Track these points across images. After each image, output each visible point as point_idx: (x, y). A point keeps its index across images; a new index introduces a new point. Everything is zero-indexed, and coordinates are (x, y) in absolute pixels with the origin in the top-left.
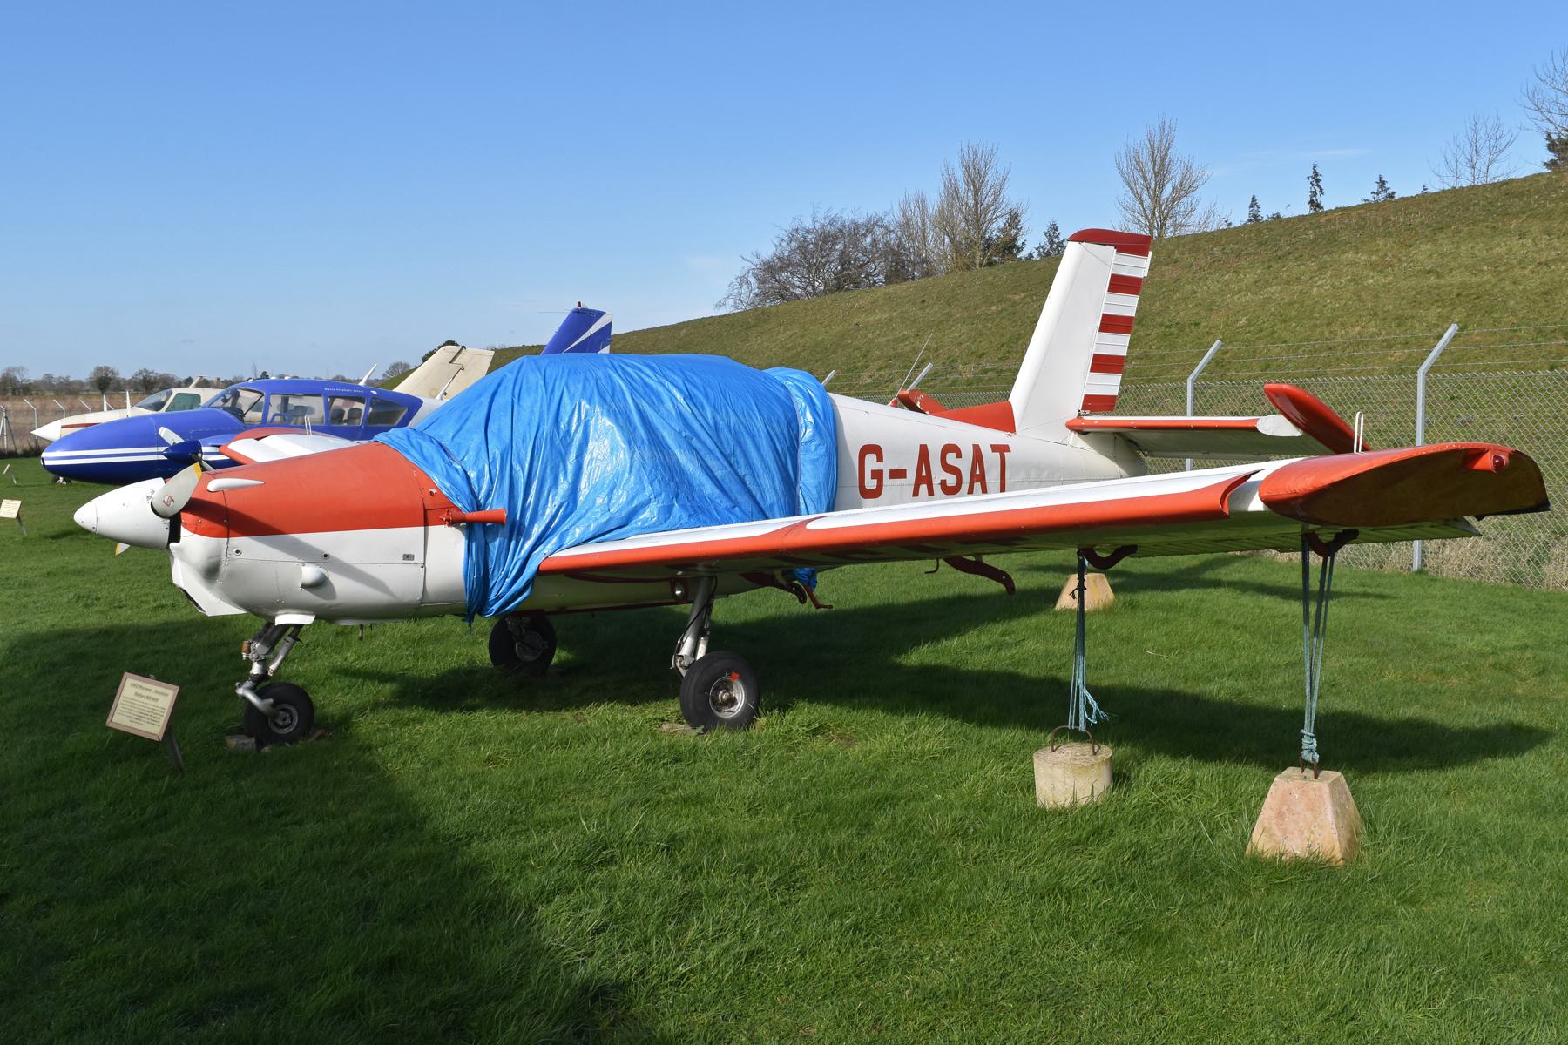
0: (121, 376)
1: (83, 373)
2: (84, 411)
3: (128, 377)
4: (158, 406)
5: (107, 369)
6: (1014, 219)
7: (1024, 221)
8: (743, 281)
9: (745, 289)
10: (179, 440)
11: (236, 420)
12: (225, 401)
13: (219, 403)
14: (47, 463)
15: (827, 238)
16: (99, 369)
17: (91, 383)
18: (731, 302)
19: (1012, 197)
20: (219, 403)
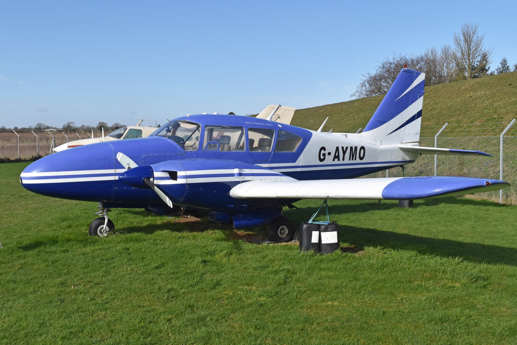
0: (108, 125)
1: (95, 124)
2: (78, 139)
3: (111, 126)
4: (119, 136)
5: (103, 123)
6: (484, 57)
7: (490, 58)
8: (363, 85)
9: (364, 88)
10: (134, 165)
11: (179, 147)
12: (168, 131)
13: (164, 132)
14: (25, 182)
15: (398, 66)
16: (100, 123)
17: (97, 128)
18: (357, 94)
19: (485, 47)
20: (164, 132)
